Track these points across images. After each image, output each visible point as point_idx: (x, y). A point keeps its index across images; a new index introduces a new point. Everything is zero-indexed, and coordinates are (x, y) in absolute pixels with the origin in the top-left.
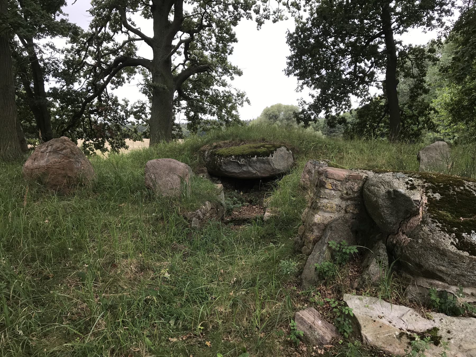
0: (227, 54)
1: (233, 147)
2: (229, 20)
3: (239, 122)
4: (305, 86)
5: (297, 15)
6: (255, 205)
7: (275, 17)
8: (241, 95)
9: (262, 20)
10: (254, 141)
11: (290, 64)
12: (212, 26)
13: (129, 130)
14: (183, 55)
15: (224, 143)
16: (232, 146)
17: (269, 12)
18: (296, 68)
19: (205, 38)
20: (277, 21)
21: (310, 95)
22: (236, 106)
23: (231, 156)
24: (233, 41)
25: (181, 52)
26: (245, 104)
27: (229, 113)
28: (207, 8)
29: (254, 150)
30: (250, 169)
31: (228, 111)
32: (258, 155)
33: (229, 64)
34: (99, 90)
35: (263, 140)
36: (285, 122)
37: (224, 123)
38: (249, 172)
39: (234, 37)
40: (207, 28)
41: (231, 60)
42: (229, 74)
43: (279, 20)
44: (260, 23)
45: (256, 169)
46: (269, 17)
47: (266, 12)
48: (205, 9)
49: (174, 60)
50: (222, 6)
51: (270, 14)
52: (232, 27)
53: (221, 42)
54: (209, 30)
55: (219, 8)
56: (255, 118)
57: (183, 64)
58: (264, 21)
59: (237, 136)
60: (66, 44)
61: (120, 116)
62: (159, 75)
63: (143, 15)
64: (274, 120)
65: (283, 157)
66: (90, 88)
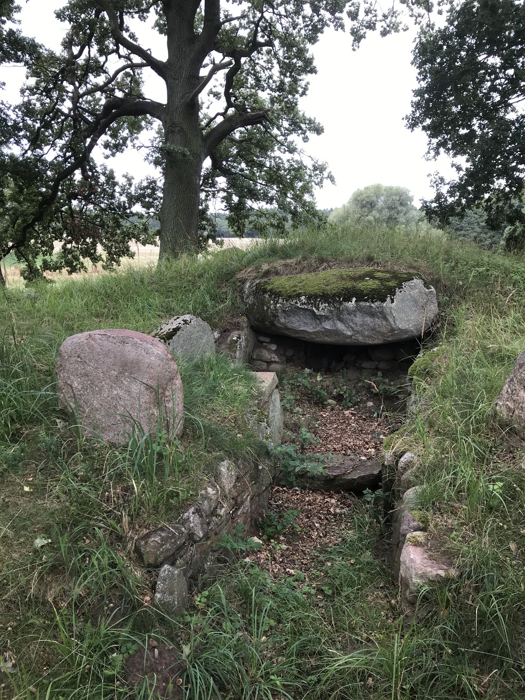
0: (297, 96)
1: (303, 276)
2: (303, 32)
3: (315, 213)
4: (442, 150)
5: (424, 22)
6: (348, 408)
7: (385, 26)
8: (319, 168)
9: (362, 32)
10: (350, 261)
11: (417, 105)
12: (272, 45)
13: (135, 226)
14: (223, 99)
15: (286, 265)
16: (301, 271)
17: (375, 16)
18: (426, 114)
19: (262, 67)
20: (389, 32)
21: (452, 166)
22: (312, 187)
23: (299, 295)
24: (309, 72)
25: (219, 94)
26: (327, 182)
27: (297, 198)
28: (265, 9)
29: (349, 284)
30: (340, 326)
31: (298, 196)
32: (360, 296)
33: (301, 113)
34: (83, 160)
35: (370, 259)
36: (386, 213)
37: (289, 216)
38: (337, 333)
39: (311, 63)
40: (265, 49)
41: (305, 106)
42: (300, 132)
43: (393, 31)
44: (358, 37)
45: (354, 326)
46: (375, 24)
47: (370, 15)
48: (262, 12)
49: (208, 108)
50: (292, 6)
51: (376, 21)
52: (308, 46)
53: (288, 74)
54: (269, 52)
55: (286, 11)
56: (340, 206)
57: (223, 114)
58: (365, 33)
59: (312, 250)
60: (27, 78)
61: (119, 204)
62: (177, 129)
63: (157, 28)
64: (369, 209)
65: (415, 301)
66: (68, 154)
